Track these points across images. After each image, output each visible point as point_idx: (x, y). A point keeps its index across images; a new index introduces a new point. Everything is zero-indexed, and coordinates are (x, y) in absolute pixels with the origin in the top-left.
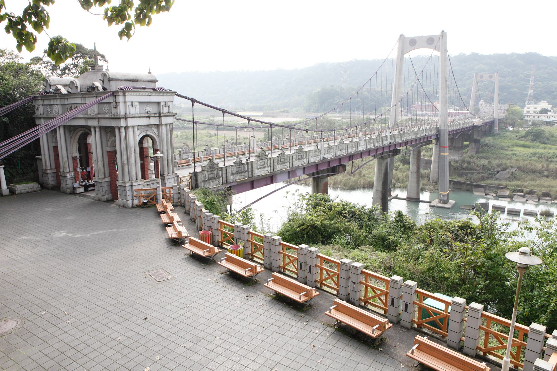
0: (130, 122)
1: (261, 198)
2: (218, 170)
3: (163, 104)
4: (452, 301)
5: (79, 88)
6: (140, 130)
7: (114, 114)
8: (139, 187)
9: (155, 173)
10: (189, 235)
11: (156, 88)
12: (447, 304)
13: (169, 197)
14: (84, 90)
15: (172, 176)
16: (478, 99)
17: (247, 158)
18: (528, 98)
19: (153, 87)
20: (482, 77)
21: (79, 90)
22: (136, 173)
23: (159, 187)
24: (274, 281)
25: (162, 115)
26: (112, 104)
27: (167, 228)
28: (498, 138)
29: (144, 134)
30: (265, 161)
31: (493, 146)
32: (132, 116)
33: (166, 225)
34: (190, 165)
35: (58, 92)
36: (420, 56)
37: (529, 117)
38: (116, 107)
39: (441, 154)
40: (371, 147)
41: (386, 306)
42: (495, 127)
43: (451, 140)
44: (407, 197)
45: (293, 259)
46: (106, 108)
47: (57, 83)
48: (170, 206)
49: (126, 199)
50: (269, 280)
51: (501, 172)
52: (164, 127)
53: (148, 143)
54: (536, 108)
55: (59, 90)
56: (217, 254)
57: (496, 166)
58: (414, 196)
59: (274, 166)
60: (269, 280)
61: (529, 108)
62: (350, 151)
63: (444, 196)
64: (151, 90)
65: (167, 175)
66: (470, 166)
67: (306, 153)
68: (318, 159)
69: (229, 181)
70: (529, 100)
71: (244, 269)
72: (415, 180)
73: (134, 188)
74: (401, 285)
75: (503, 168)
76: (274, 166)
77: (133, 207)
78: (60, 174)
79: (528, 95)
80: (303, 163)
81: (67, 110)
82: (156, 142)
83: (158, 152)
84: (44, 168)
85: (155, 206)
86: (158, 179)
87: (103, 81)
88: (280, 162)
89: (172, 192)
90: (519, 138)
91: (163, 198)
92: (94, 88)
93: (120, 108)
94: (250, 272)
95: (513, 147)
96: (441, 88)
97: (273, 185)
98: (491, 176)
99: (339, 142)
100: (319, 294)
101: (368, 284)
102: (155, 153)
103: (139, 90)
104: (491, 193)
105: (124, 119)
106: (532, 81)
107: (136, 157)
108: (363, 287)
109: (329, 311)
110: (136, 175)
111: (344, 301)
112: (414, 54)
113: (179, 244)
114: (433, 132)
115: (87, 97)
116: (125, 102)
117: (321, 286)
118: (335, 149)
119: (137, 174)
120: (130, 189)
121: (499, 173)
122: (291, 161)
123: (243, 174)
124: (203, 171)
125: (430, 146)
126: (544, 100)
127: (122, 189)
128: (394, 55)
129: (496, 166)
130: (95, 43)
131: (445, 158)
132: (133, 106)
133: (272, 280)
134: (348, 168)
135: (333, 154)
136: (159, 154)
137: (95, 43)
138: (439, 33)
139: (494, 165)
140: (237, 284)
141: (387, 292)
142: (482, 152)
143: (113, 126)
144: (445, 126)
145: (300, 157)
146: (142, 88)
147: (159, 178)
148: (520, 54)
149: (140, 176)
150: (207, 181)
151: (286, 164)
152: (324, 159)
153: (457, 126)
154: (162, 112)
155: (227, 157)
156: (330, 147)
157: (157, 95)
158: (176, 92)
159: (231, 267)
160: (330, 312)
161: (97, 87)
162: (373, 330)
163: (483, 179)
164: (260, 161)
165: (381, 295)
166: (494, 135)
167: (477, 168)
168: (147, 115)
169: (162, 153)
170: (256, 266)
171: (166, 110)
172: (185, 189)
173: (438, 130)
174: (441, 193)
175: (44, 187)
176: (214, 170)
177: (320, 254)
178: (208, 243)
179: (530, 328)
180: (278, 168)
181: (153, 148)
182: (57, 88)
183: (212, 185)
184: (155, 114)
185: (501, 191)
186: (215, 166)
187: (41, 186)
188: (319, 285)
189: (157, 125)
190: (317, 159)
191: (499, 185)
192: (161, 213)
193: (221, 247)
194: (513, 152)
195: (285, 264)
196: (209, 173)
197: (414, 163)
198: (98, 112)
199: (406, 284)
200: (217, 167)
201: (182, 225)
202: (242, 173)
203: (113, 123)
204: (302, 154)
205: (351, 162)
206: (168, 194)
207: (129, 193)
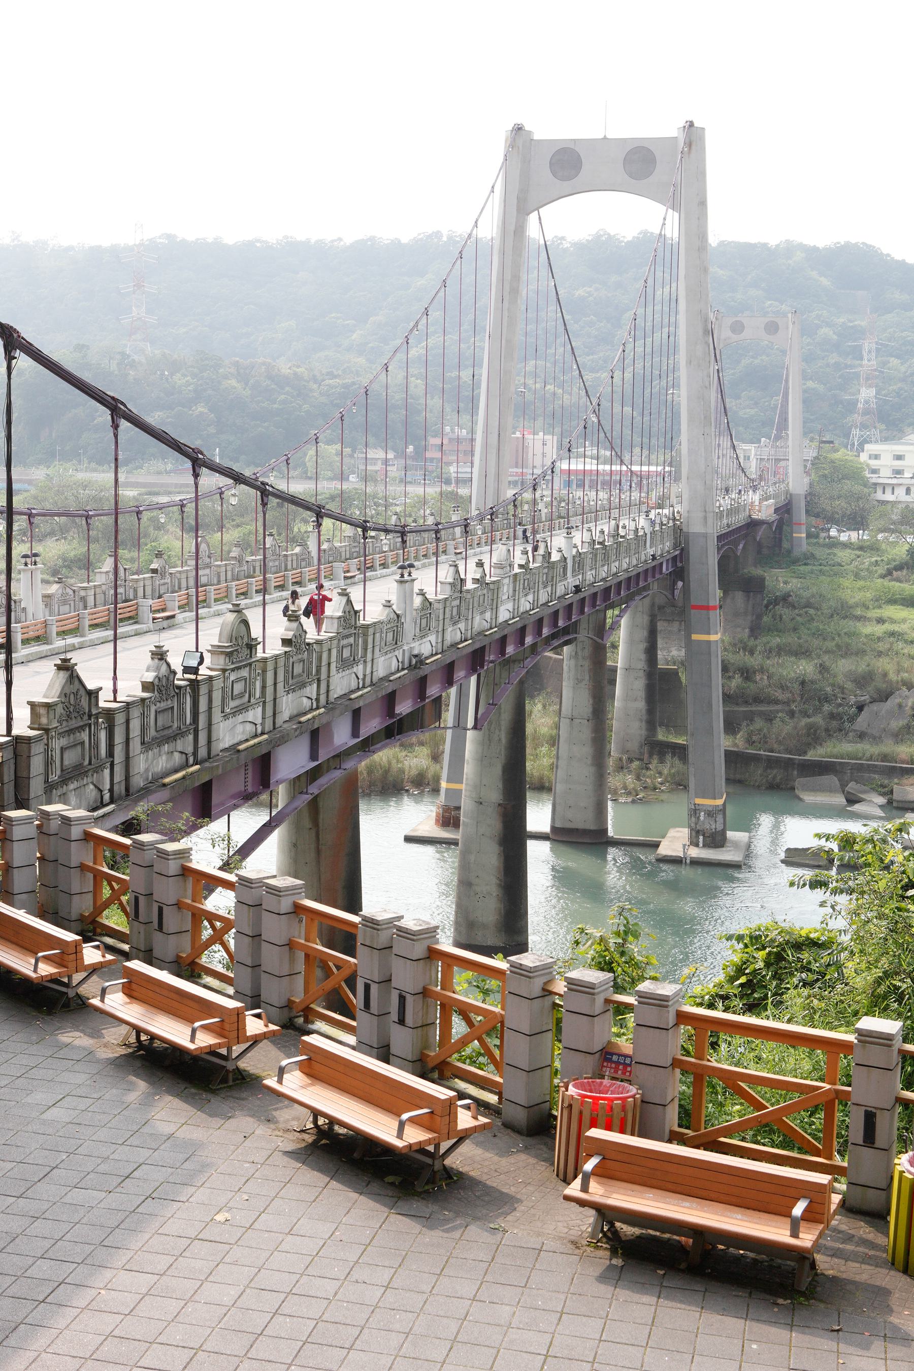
17: (194, 663)
18: (857, 418)
28: (812, 572)
31: (808, 605)
36: (438, 234)
37: (888, 490)
39: (695, 637)
42: (795, 527)
44: (553, 828)
51: (875, 707)
54: (899, 457)
57: (849, 685)
58: (583, 820)
61: (877, 457)
63: (710, 814)
66: (752, 688)
67: (365, 635)
69: (138, 782)
70: (864, 426)
72: (587, 750)
75: (879, 691)
79: (860, 405)
90: (889, 573)
95: (880, 607)
96: (689, 362)
104: (865, 792)
106: (870, 352)
121: (866, 709)
129: (849, 685)
131: (709, 654)
139: (840, 679)
142: (778, 630)
144: (705, 518)
148: (815, 249)
164: (233, 677)
166: (795, 562)
167: (779, 695)
174: (698, 801)
176: (81, 728)
185: (905, 781)
191: (885, 757)
194: (887, 627)
197: (578, 681)
200: (94, 712)
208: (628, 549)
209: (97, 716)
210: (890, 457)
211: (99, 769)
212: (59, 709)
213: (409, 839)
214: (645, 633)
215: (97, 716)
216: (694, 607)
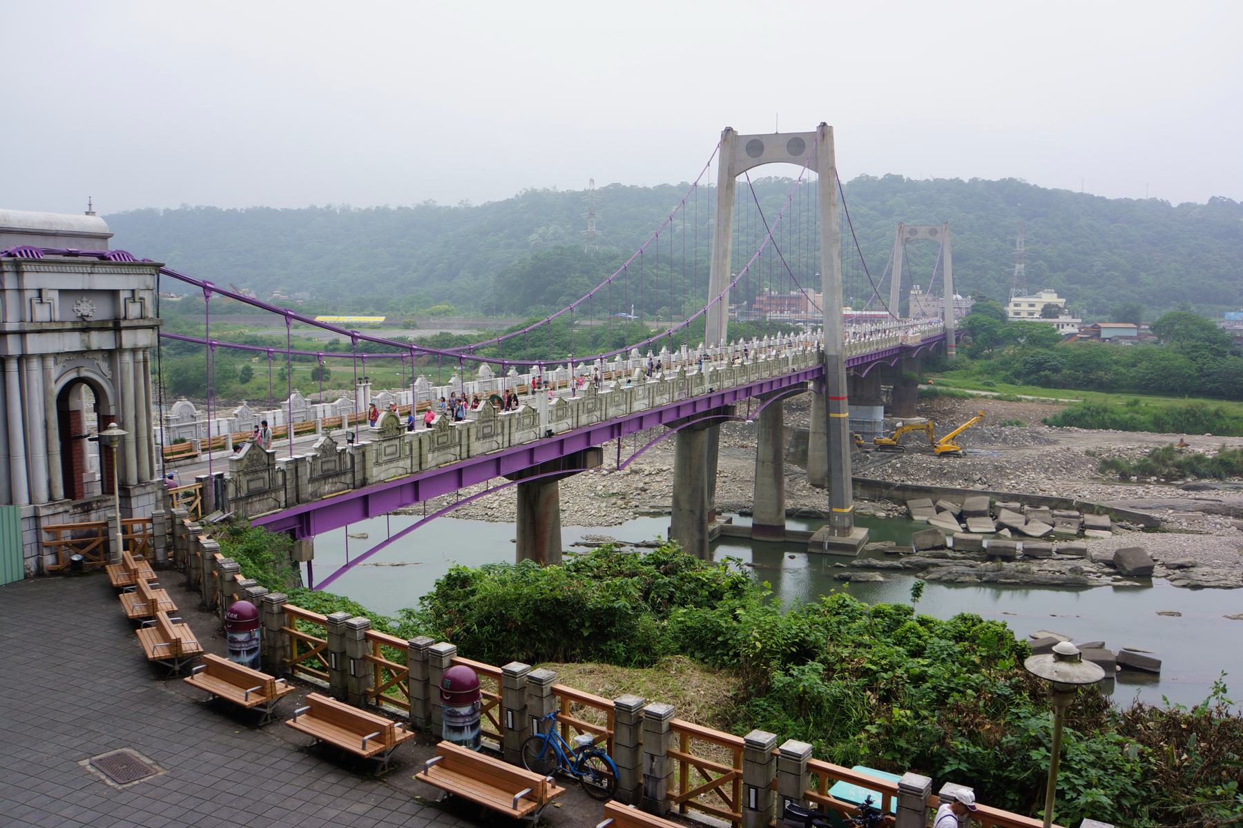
0: (35, 344)
3: (128, 295)
4: (899, 784)
6: (60, 366)
9: (102, 480)
10: (201, 650)
11: (107, 254)
12: (887, 791)
13: (141, 546)
16: (908, 282)
19: (98, 250)
20: (913, 232)
22: (50, 483)
23: (114, 519)
24: (310, 713)
25: (123, 324)
27: (138, 631)
29: (73, 375)
30: (396, 442)
32: (39, 327)
33: (135, 624)
34: (196, 456)
39: (831, 415)
40: (665, 401)
41: (735, 810)
42: (949, 348)
43: (854, 381)
45: (721, 775)
48: (145, 572)
50: (297, 711)
52: (127, 358)
53: (85, 401)
54: (1032, 305)
56: (282, 696)
59: (420, 455)
62: (612, 412)
64: (95, 259)
65: (135, 487)
69: (303, 496)
70: (1018, 286)
71: (508, 795)
73: (44, 523)
74: (773, 754)
76: (420, 455)
79: (1015, 274)
83: (113, 424)
85: (103, 570)
86: (111, 497)
88: (436, 446)
89: (150, 531)
91: (126, 548)
94: (375, 743)
99: (585, 391)
100: (562, 793)
101: (380, 659)
102: (102, 428)
103: (61, 258)
107: (51, 437)
108: (677, 765)
111: (631, 807)
112: (758, 174)
113: (174, 673)
116: (20, 291)
117: (683, 810)
118: (575, 409)
119: (53, 485)
120: (33, 527)
122: (464, 442)
125: (803, 397)
126: (1048, 286)
128: (712, 179)
132: (42, 302)
133: (306, 712)
134: (609, 460)
135: (569, 421)
136: (114, 431)
138: (812, 127)
141: (737, 773)
145: (486, 431)
146: (70, 254)
147: (113, 493)
149: (60, 492)
150: (241, 499)
151: (452, 450)
152: (550, 434)
153: (865, 347)
155: (296, 433)
156: (562, 405)
157: (107, 273)
158: (163, 265)
159: (499, 801)
162: (515, 802)
164: (385, 444)
165: (722, 782)
169: (122, 426)
170: (391, 727)
172: (187, 522)
173: (822, 356)
177: (679, 722)
179: (745, 740)
181: (98, 415)
183: (262, 510)
186: (265, 458)
188: (678, 807)
189: (109, 351)
192: (119, 590)
193: (291, 679)
195: (379, 686)
196: (248, 478)
201: (181, 622)
204: (492, 423)
205: (616, 441)
206: (138, 536)
208: (856, 347)
210: (1027, 305)
213: (1179, 615)
216: (219, 434)
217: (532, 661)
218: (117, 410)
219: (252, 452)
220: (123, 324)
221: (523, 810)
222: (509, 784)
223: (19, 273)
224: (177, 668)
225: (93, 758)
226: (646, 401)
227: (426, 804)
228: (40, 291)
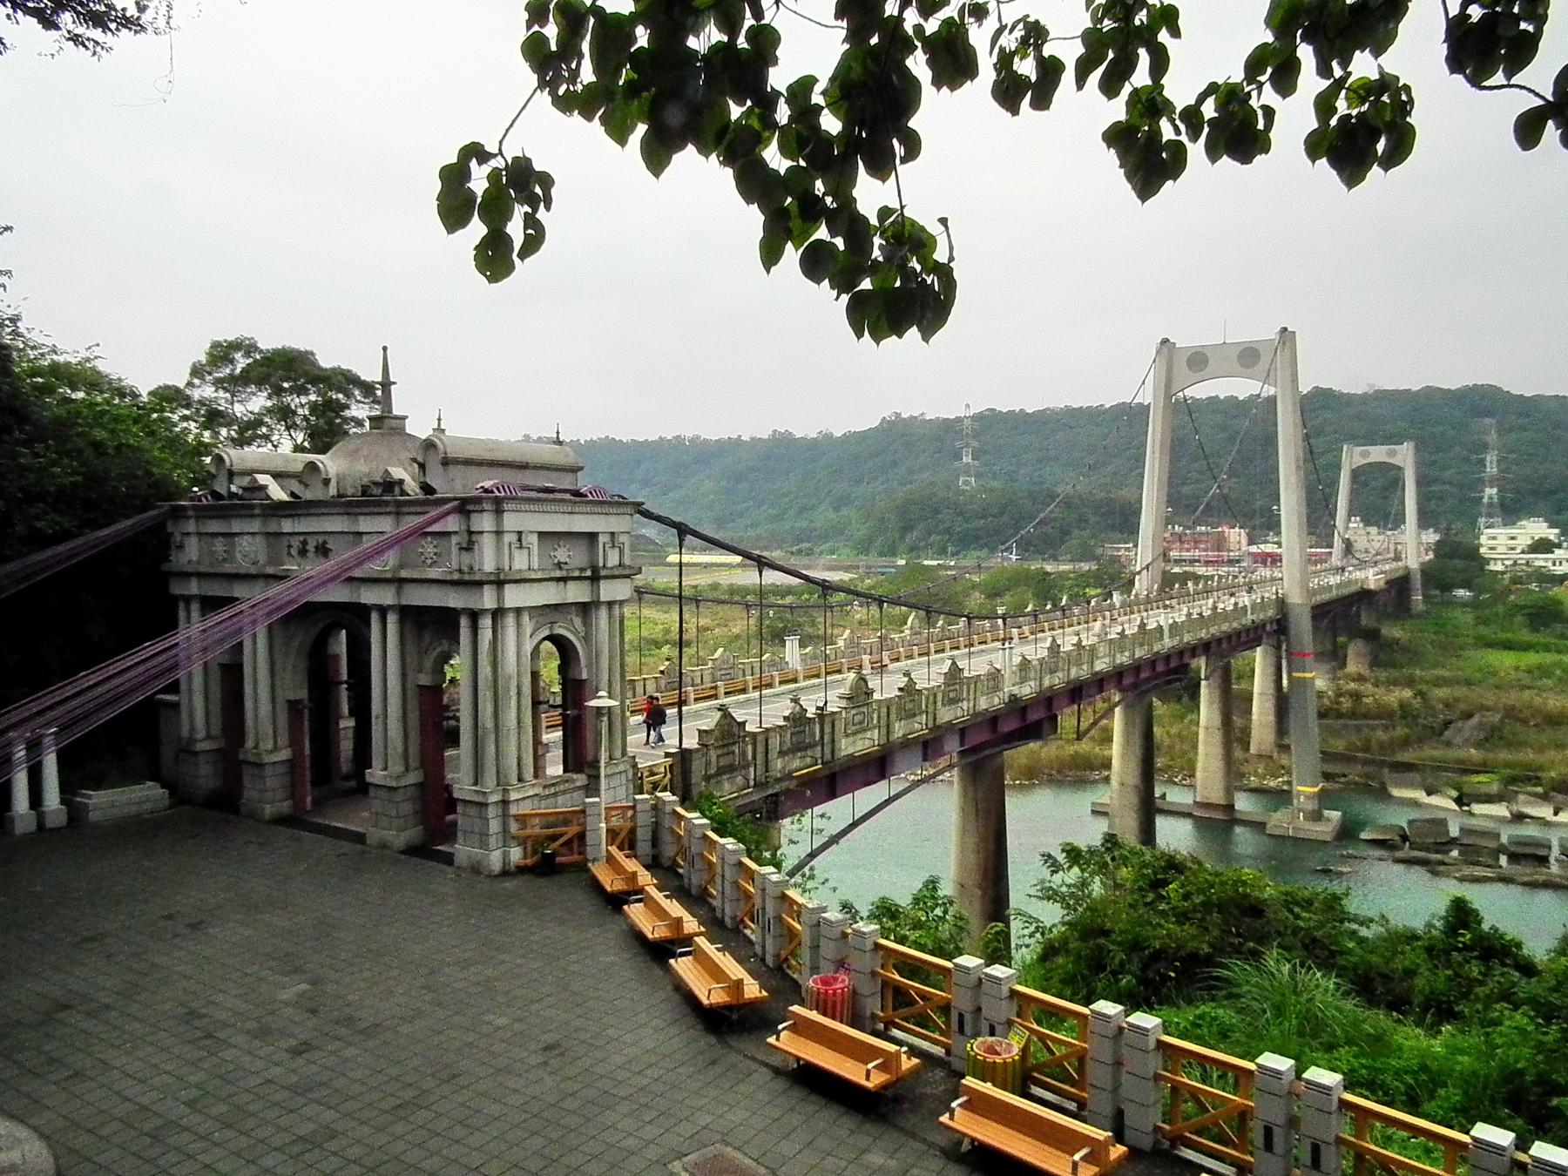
0: (514, 597)
1: (854, 825)
2: (744, 741)
5: (333, 483)
6: (534, 621)
7: (460, 571)
8: (525, 808)
14: (350, 491)
15: (621, 768)
17: (822, 704)
21: (333, 491)
22: (519, 759)
24: (793, 1029)
25: (603, 573)
26: (454, 540)
30: (865, 709)
35: (257, 494)
38: (468, 547)
39: (1294, 674)
46: (430, 550)
47: (255, 465)
49: (484, 845)
55: (263, 488)
60: (780, 1027)
68: (996, 701)
70: (1490, 515)
73: (513, 810)
77: (505, 873)
78: (241, 757)
79: (1485, 500)
80: (959, 714)
81: (289, 554)
82: (579, 660)
84: (185, 731)
85: (582, 867)
87: (422, 466)
91: (611, 841)
92: (390, 485)
93: (481, 550)
97: (883, 784)
98: (1437, 732)
103: (533, 494)
105: (494, 586)
109: (947, 1115)
110: (519, 765)
111: (989, 1085)
114: (1271, 613)
115: (361, 514)
120: (500, 813)
122: (931, 708)
123: (809, 753)
124: (704, 745)
127: (473, 811)
130: (385, 349)
135: (1032, 683)
137: (385, 349)
140: (824, 1102)
143: (454, 609)
145: (952, 695)
151: (918, 719)
154: (601, 565)
160: (952, 1118)
161: (401, 482)
162: (868, 1073)
163: (1405, 743)
164: (853, 712)
168: (558, 574)
170: (898, 1054)
171: (613, 559)
175: (179, 794)
176: (734, 743)
178: (841, 1022)
179: (1257, 1064)
180: (899, 730)
182: (256, 481)
184: (582, 570)
187: (171, 794)
189: (584, 604)
190: (996, 701)
198: (397, 563)
199: (1130, 1025)
202: (806, 749)
203: (454, 600)
204: (957, 687)
205: (1076, 707)
207: (494, 826)
209: (745, 737)
211: (746, 767)
212: (717, 733)
214: (1273, 669)
215: (745, 737)
217: (1134, 1002)
218: (589, 672)
219: (723, 723)
220: (603, 573)
221: (877, 1082)
222: (862, 1053)
223: (499, 512)
224: (735, 1017)
225: (685, 1159)
226: (1107, 660)
227: (777, 1072)
228: (520, 533)
